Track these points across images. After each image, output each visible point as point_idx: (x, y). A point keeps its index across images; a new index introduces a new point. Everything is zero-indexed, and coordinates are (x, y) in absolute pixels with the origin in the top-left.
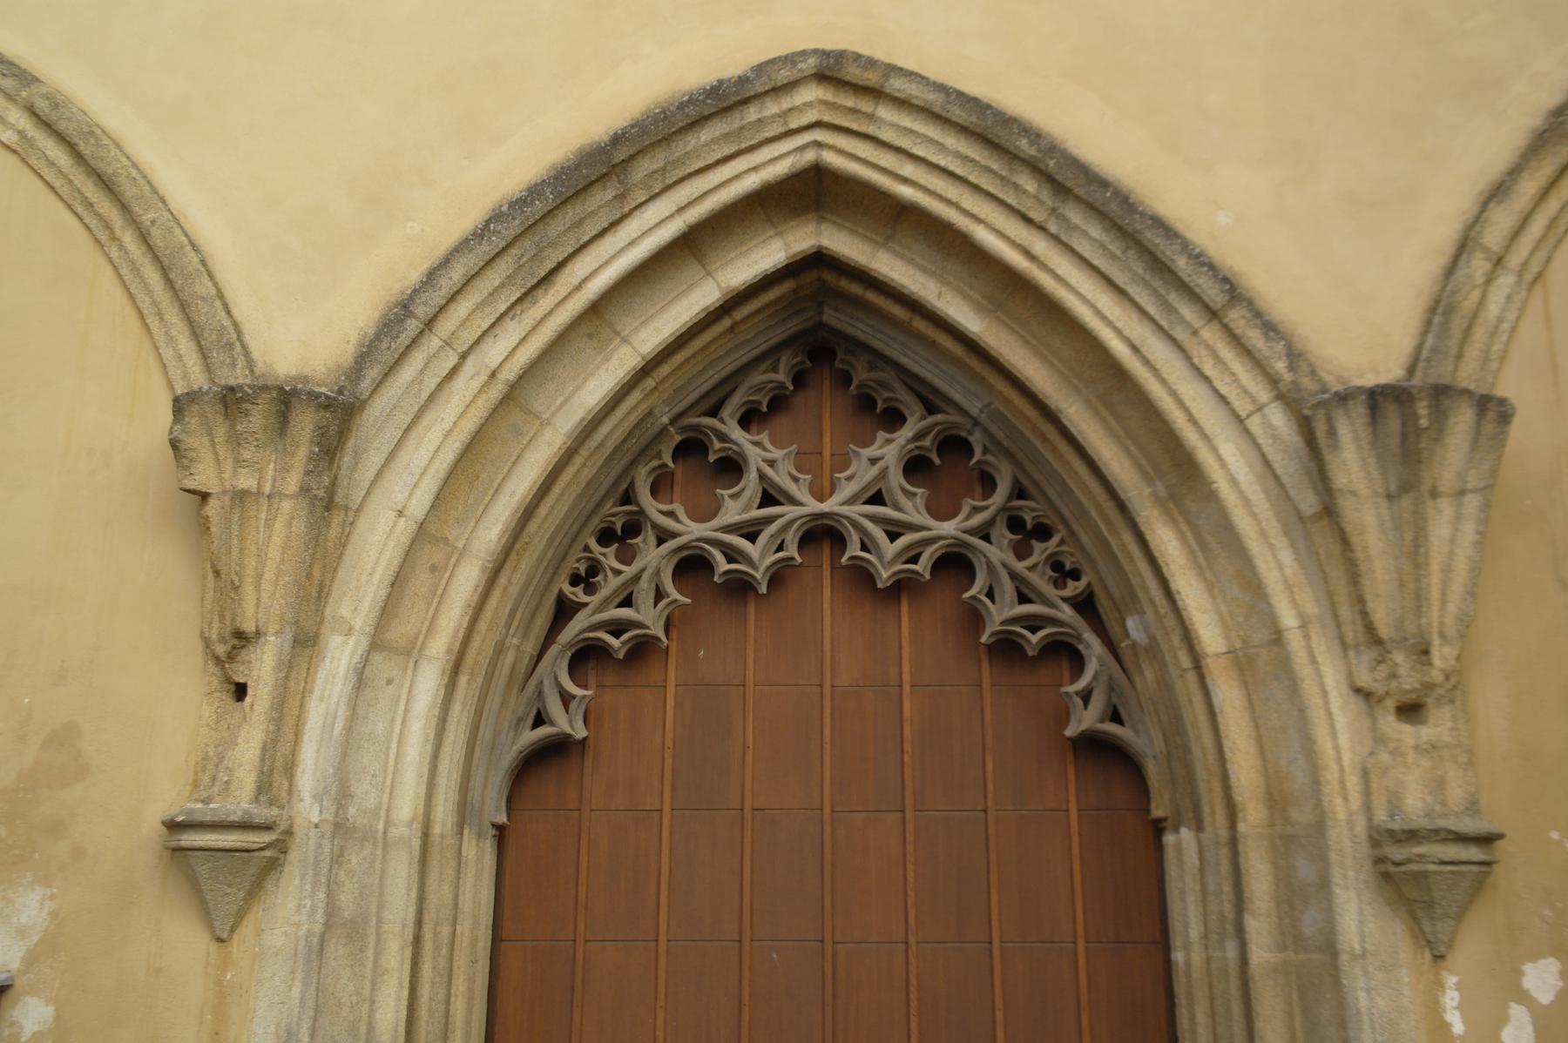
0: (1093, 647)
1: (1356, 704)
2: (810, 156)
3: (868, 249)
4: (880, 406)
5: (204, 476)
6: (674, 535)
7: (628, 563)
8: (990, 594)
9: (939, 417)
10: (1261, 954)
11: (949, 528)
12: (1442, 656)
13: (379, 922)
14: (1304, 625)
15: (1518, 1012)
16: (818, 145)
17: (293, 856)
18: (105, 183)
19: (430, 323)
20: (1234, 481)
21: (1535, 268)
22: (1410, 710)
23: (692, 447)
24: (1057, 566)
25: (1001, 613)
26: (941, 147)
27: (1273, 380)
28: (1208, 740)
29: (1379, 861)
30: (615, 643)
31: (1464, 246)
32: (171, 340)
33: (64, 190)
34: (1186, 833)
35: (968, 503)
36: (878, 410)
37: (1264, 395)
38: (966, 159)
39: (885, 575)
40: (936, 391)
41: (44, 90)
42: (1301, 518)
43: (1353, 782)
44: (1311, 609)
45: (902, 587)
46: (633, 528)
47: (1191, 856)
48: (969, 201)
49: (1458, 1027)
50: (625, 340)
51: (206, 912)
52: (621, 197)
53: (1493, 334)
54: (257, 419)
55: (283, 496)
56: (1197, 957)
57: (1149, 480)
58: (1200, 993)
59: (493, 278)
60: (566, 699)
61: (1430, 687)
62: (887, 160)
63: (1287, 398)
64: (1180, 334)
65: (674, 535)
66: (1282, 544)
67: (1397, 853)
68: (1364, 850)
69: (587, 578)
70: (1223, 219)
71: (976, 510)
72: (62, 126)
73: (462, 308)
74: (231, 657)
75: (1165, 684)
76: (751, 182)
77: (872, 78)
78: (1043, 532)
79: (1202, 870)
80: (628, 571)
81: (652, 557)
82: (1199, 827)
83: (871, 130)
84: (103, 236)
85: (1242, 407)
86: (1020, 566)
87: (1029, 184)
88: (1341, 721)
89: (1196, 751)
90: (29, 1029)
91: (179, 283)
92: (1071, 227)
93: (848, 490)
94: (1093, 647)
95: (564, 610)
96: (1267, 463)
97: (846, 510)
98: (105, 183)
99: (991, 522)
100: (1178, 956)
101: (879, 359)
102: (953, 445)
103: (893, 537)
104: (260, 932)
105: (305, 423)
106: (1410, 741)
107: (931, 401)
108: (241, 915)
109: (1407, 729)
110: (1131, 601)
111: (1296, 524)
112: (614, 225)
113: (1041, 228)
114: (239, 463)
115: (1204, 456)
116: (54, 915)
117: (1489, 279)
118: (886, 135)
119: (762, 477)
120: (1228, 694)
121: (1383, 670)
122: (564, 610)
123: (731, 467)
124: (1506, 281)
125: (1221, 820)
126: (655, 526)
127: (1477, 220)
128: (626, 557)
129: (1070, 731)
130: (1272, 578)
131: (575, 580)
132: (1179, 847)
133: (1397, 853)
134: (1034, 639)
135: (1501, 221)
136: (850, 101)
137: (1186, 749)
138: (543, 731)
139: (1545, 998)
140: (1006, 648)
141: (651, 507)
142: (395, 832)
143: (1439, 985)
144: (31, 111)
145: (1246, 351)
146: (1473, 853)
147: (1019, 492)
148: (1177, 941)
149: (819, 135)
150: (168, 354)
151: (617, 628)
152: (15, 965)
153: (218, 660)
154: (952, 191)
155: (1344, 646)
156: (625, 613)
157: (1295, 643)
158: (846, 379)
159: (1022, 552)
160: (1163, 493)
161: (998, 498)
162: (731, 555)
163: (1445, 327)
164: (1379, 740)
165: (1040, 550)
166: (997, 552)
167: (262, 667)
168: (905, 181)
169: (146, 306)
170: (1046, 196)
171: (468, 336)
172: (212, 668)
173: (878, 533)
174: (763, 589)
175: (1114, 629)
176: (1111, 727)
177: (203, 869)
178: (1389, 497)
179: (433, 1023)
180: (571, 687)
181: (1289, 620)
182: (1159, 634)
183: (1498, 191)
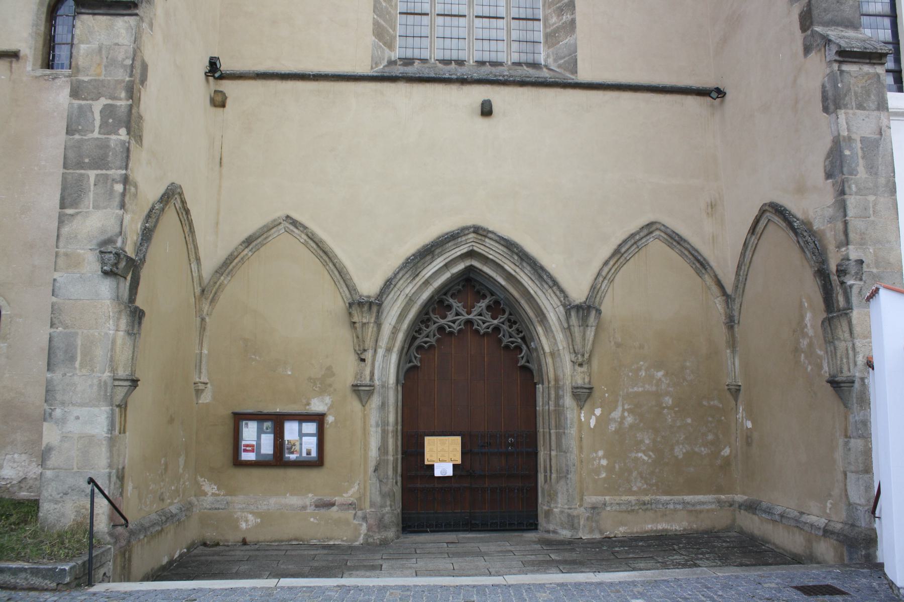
0: (524, 347)
1: (571, 363)
2: (471, 248)
3: (482, 265)
4: (481, 294)
5: (356, 319)
6: (437, 323)
7: (427, 328)
8: (504, 336)
9: (494, 297)
10: (552, 408)
11: (496, 322)
12: (586, 356)
13: (388, 403)
14: (564, 348)
15: (593, 417)
16: (473, 246)
17: (375, 391)
18: (325, 253)
19: (395, 286)
20: (552, 320)
21: (612, 279)
22: (581, 365)
23: (441, 302)
24: (517, 330)
25: (506, 340)
26: (498, 249)
27: (561, 302)
28: (545, 368)
29: (573, 392)
30: (426, 346)
31: (599, 274)
32: (342, 287)
33: (316, 253)
34: (540, 385)
35: (500, 316)
36: (502, 345)
37: (559, 304)
38: (503, 251)
39: (482, 332)
40: (494, 292)
41: (310, 231)
42: (564, 329)
43: (569, 378)
44: (565, 346)
45: (486, 334)
46: (429, 320)
47: (541, 390)
48: (504, 259)
49: (583, 420)
50: (431, 285)
51: (361, 400)
52: (432, 258)
53: (602, 293)
54: (366, 308)
55: (371, 323)
56: (541, 408)
57: (537, 317)
58: (541, 415)
59: (407, 275)
60: (416, 357)
61: (584, 361)
62: (487, 250)
63: (564, 306)
64: (544, 291)
65: (437, 323)
66: (561, 333)
67: (575, 391)
68: (571, 390)
69: (419, 331)
70: (554, 266)
71: (501, 318)
72: (315, 239)
73: (401, 282)
74: (361, 354)
75: (538, 356)
76: (459, 253)
77: (485, 233)
78: (515, 323)
79: (543, 392)
80: (428, 330)
81: (433, 327)
82: (543, 384)
83: (484, 244)
84: (325, 264)
85: (555, 306)
86: (510, 330)
87: (516, 258)
88: (568, 367)
89: (543, 369)
90: (330, 422)
91: (343, 276)
92: (524, 267)
93: (475, 313)
94: (524, 347)
95: (414, 339)
96: (559, 317)
97: (474, 318)
98: (325, 253)
99: (505, 321)
100: (538, 408)
101: (481, 284)
102: (497, 303)
103: (484, 323)
104: (370, 405)
105: (375, 309)
106: (579, 371)
107: (492, 294)
108: (367, 402)
109: (579, 368)
110: (532, 339)
111: (563, 329)
112: (431, 263)
113: (518, 266)
114: (362, 316)
115: (547, 315)
116: (332, 401)
117: (603, 282)
118: (487, 245)
119: (456, 310)
120: (549, 360)
121: (576, 358)
122: (414, 339)
123: (449, 307)
124: (606, 281)
125: (547, 383)
126: (434, 320)
127: (601, 270)
128: (427, 327)
129: (519, 365)
130: (558, 339)
131: (416, 332)
132: (539, 388)
133: (575, 391)
134: (513, 346)
135: (606, 270)
136: (480, 237)
137: (541, 369)
138: (411, 364)
139: (598, 415)
140: (507, 347)
141: (433, 316)
142: (389, 386)
143: (581, 413)
144: (307, 235)
145: (556, 295)
146: (588, 391)
147: (510, 314)
148: (538, 405)
149: (473, 244)
150: (341, 290)
151: (426, 342)
152: (326, 410)
153: (358, 354)
154: (500, 257)
155: (570, 353)
156: (427, 339)
157: (561, 352)
158: (474, 287)
159: (511, 327)
160: (539, 320)
161: (506, 316)
162: (450, 327)
163: (593, 292)
164: (574, 370)
165: (515, 327)
166: (505, 327)
167: (368, 356)
168: (491, 254)
169: (335, 279)
170: (519, 260)
171: (402, 288)
172: (356, 355)
173: (481, 322)
174: (456, 335)
175: (529, 345)
176: (527, 364)
177: (362, 393)
178: (579, 326)
179: (76, 503)
180: (416, 355)
181: (561, 348)
182: (538, 346)
183: (606, 263)
